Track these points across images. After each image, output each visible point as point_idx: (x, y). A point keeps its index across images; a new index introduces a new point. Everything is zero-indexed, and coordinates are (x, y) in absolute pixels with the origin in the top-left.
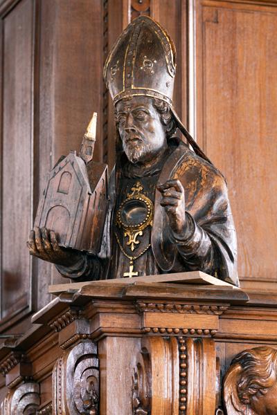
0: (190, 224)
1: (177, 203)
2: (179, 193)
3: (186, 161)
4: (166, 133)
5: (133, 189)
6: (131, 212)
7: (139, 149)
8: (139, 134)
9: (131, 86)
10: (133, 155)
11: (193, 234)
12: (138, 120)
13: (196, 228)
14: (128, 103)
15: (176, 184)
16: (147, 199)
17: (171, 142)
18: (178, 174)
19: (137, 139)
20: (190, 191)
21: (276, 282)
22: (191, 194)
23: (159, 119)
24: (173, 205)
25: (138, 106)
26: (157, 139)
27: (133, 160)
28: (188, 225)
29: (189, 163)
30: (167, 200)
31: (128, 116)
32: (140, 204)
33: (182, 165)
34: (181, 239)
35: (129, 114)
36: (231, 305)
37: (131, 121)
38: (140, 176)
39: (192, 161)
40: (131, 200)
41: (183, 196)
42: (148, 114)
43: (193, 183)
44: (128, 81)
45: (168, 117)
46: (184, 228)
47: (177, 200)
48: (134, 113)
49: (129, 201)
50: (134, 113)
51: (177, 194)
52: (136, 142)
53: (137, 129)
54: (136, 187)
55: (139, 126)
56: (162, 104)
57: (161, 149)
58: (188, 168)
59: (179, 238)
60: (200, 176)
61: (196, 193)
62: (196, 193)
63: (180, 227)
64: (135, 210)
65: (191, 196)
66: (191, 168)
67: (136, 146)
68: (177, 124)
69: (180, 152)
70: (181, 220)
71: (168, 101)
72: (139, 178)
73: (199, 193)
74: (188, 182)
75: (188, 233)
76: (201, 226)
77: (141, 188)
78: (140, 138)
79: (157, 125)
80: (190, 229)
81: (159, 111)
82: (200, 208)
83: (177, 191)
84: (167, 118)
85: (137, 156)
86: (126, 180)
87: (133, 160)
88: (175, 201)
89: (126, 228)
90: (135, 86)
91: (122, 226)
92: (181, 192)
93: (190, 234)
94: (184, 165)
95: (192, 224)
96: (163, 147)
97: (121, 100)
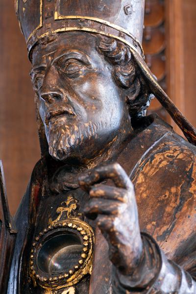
0: (152, 256)
1: (116, 209)
2: (121, 190)
3: (163, 151)
4: (128, 102)
5: (60, 209)
6: (56, 255)
7: (68, 132)
8: (69, 103)
9: (53, 15)
10: (58, 143)
11: (157, 275)
12: (67, 79)
13: (164, 266)
14: (49, 46)
15: (113, 171)
16: (84, 224)
17: (136, 122)
18: (145, 175)
19: (65, 113)
20: (167, 204)
21: (194, 250)
22: (168, 209)
23: (110, 74)
24: (108, 214)
25: (65, 50)
26: (110, 114)
27: (58, 152)
28: (147, 257)
29: (167, 154)
30: (96, 204)
31: (47, 70)
32: (71, 237)
33: (153, 158)
34: (133, 285)
35: (49, 67)
36: (53, 218)
37: (53, 80)
38: (73, 185)
39: (175, 150)
40: (54, 228)
41: (130, 196)
42: (87, 64)
43: (173, 190)
44: (48, 7)
45: (130, 70)
46: (140, 263)
47: (120, 204)
48: (58, 63)
49: (50, 230)
50: (58, 63)
51: (116, 192)
52: (64, 119)
53: (65, 95)
54: (65, 205)
55: (71, 90)
56: (114, 44)
57: (115, 133)
58: (165, 163)
59: (128, 284)
60: (190, 177)
61: (178, 209)
62: (178, 209)
63: (130, 262)
64: (63, 250)
65: (169, 214)
66: (172, 163)
67: (63, 127)
68: (148, 87)
69: (152, 134)
70: (129, 245)
71: (129, 42)
72: (72, 189)
73: (185, 208)
74: (164, 188)
75: (147, 275)
76: (187, 271)
77: (74, 207)
78: (70, 111)
79: (106, 91)
80: (152, 266)
81: (110, 58)
82: (186, 236)
83: (117, 186)
84: (126, 73)
85: (65, 146)
86: (53, 199)
87: (58, 152)
88: (112, 206)
89: (43, 283)
90: (61, 14)
91: (38, 280)
92: (125, 187)
93: (152, 276)
94: (158, 157)
95: (156, 255)
96: (120, 128)
97: (36, 44)
